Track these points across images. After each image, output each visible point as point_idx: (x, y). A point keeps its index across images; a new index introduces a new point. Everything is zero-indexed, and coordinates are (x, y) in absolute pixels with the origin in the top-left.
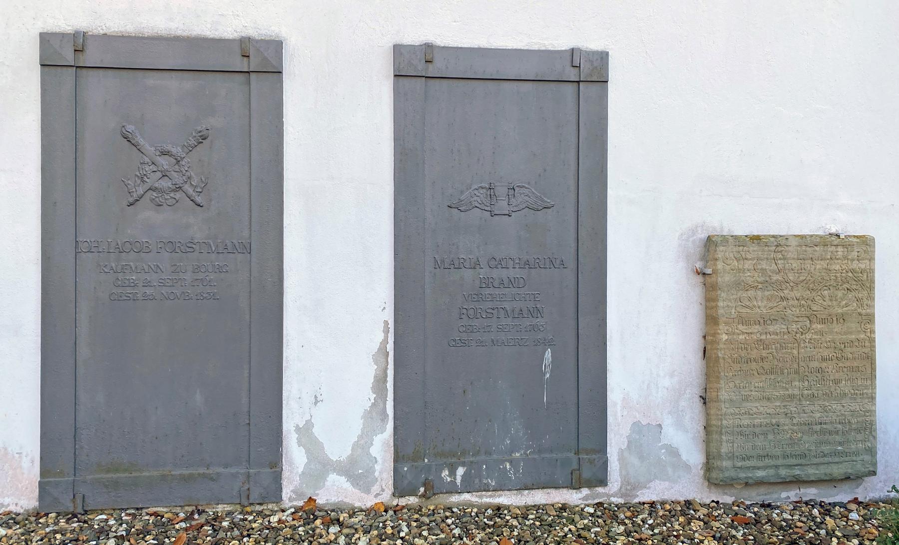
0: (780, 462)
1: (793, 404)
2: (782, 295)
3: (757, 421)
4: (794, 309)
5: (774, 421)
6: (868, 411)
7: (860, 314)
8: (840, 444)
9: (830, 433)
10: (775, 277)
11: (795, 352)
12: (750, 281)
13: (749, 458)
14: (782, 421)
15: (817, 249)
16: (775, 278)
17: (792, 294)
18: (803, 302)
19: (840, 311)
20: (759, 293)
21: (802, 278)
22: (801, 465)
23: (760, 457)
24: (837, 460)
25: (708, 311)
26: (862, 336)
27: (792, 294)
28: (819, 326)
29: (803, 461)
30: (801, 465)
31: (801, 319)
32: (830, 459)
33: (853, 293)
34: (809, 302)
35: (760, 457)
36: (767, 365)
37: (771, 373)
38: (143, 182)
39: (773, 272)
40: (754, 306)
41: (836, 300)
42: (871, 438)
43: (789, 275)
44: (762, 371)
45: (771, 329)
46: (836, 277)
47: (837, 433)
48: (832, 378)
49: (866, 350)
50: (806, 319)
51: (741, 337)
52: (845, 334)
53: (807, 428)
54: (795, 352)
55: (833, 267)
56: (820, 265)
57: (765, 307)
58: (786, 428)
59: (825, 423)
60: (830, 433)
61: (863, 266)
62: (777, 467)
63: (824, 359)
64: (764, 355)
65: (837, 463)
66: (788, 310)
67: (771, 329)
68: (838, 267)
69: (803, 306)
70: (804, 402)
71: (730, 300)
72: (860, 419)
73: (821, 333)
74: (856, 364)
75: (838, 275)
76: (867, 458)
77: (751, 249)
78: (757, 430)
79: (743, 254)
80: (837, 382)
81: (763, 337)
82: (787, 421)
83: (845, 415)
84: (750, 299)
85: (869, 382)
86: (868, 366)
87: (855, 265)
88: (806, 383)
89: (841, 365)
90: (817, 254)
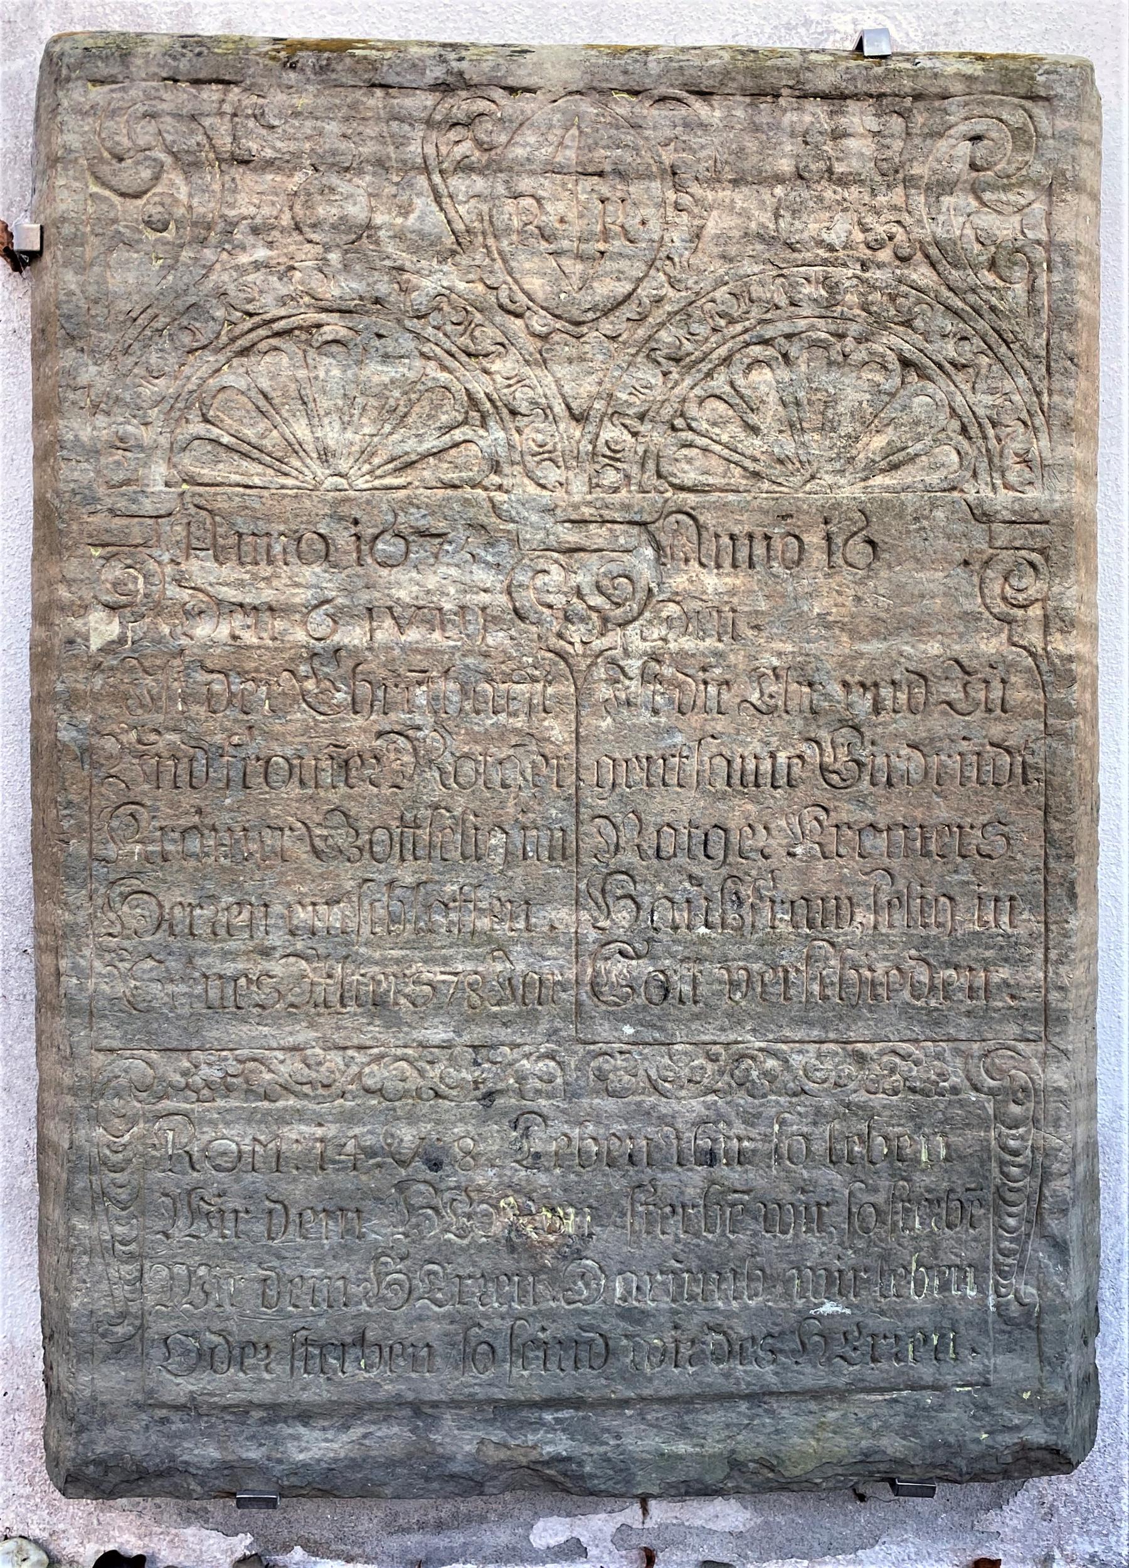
0: (438, 1382)
1: (536, 1039)
2: (480, 387)
3: (297, 1135)
4: (553, 475)
5: (407, 1135)
6: (1022, 1093)
7: (981, 515)
8: (835, 1283)
9: (770, 1214)
10: (433, 280)
11: (557, 730)
12: (268, 296)
13: (241, 1352)
14: (461, 1135)
15: (709, 112)
16: (429, 285)
17: (544, 384)
18: (611, 433)
19: (849, 490)
20: (331, 370)
21: (606, 289)
22: (577, 1403)
23: (315, 1350)
24: (810, 1375)
25: (105, 1381)
26: (991, 645)
27: (544, 384)
28: (712, 582)
29: (591, 1381)
30: (577, 1403)
31: (598, 535)
32: (768, 1373)
33: (940, 388)
34: (656, 437)
35: (315, 1350)
36: (370, 802)
37: (405, 848)
38: (590, 1235)
39: (421, 243)
40: (295, 448)
41: (827, 427)
42: (1042, 1254)
43: (524, 263)
44: (341, 838)
45: (405, 585)
46: (832, 287)
47: (815, 1215)
48: (791, 888)
49: (1015, 731)
50: (626, 536)
51: (203, 630)
52: (882, 628)
53: (618, 1182)
54: (557, 730)
55: (812, 226)
56: (730, 212)
57: (366, 453)
58: (484, 1177)
59: (741, 1158)
60: (770, 1214)
61: (1005, 228)
62: (420, 1411)
63: (744, 782)
64: (355, 742)
65: (816, 1395)
66: (513, 477)
67: (405, 585)
68: (840, 230)
69: (614, 456)
70: (604, 1030)
71: (137, 410)
72: (967, 1140)
73: (727, 622)
74: (943, 812)
75: (844, 275)
76: (1012, 1368)
77: (279, 98)
78: (298, 1189)
79: (222, 131)
80: (819, 913)
81: (353, 636)
82: (495, 1137)
83: (867, 1113)
84: (265, 405)
85: (1029, 922)
86: (1027, 823)
87: (957, 219)
88: (623, 915)
89: (847, 812)
90: (709, 148)
